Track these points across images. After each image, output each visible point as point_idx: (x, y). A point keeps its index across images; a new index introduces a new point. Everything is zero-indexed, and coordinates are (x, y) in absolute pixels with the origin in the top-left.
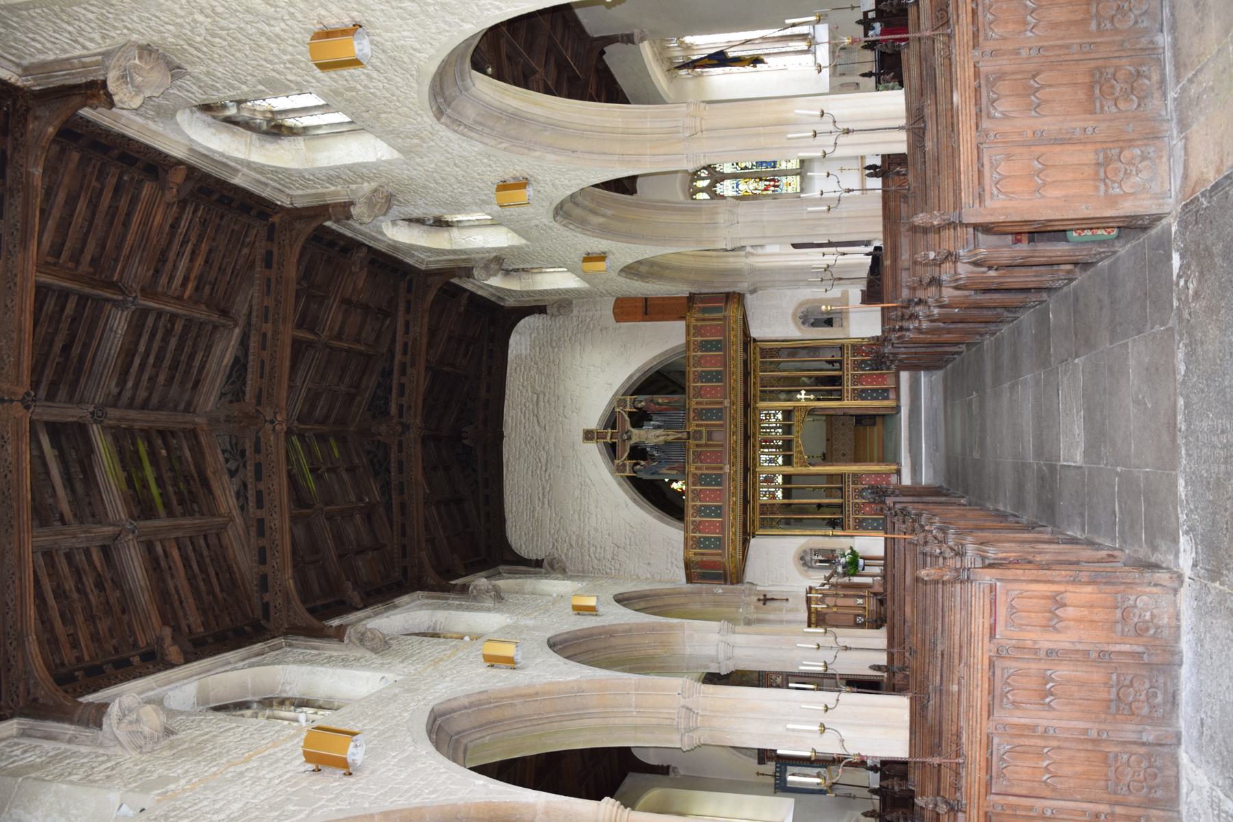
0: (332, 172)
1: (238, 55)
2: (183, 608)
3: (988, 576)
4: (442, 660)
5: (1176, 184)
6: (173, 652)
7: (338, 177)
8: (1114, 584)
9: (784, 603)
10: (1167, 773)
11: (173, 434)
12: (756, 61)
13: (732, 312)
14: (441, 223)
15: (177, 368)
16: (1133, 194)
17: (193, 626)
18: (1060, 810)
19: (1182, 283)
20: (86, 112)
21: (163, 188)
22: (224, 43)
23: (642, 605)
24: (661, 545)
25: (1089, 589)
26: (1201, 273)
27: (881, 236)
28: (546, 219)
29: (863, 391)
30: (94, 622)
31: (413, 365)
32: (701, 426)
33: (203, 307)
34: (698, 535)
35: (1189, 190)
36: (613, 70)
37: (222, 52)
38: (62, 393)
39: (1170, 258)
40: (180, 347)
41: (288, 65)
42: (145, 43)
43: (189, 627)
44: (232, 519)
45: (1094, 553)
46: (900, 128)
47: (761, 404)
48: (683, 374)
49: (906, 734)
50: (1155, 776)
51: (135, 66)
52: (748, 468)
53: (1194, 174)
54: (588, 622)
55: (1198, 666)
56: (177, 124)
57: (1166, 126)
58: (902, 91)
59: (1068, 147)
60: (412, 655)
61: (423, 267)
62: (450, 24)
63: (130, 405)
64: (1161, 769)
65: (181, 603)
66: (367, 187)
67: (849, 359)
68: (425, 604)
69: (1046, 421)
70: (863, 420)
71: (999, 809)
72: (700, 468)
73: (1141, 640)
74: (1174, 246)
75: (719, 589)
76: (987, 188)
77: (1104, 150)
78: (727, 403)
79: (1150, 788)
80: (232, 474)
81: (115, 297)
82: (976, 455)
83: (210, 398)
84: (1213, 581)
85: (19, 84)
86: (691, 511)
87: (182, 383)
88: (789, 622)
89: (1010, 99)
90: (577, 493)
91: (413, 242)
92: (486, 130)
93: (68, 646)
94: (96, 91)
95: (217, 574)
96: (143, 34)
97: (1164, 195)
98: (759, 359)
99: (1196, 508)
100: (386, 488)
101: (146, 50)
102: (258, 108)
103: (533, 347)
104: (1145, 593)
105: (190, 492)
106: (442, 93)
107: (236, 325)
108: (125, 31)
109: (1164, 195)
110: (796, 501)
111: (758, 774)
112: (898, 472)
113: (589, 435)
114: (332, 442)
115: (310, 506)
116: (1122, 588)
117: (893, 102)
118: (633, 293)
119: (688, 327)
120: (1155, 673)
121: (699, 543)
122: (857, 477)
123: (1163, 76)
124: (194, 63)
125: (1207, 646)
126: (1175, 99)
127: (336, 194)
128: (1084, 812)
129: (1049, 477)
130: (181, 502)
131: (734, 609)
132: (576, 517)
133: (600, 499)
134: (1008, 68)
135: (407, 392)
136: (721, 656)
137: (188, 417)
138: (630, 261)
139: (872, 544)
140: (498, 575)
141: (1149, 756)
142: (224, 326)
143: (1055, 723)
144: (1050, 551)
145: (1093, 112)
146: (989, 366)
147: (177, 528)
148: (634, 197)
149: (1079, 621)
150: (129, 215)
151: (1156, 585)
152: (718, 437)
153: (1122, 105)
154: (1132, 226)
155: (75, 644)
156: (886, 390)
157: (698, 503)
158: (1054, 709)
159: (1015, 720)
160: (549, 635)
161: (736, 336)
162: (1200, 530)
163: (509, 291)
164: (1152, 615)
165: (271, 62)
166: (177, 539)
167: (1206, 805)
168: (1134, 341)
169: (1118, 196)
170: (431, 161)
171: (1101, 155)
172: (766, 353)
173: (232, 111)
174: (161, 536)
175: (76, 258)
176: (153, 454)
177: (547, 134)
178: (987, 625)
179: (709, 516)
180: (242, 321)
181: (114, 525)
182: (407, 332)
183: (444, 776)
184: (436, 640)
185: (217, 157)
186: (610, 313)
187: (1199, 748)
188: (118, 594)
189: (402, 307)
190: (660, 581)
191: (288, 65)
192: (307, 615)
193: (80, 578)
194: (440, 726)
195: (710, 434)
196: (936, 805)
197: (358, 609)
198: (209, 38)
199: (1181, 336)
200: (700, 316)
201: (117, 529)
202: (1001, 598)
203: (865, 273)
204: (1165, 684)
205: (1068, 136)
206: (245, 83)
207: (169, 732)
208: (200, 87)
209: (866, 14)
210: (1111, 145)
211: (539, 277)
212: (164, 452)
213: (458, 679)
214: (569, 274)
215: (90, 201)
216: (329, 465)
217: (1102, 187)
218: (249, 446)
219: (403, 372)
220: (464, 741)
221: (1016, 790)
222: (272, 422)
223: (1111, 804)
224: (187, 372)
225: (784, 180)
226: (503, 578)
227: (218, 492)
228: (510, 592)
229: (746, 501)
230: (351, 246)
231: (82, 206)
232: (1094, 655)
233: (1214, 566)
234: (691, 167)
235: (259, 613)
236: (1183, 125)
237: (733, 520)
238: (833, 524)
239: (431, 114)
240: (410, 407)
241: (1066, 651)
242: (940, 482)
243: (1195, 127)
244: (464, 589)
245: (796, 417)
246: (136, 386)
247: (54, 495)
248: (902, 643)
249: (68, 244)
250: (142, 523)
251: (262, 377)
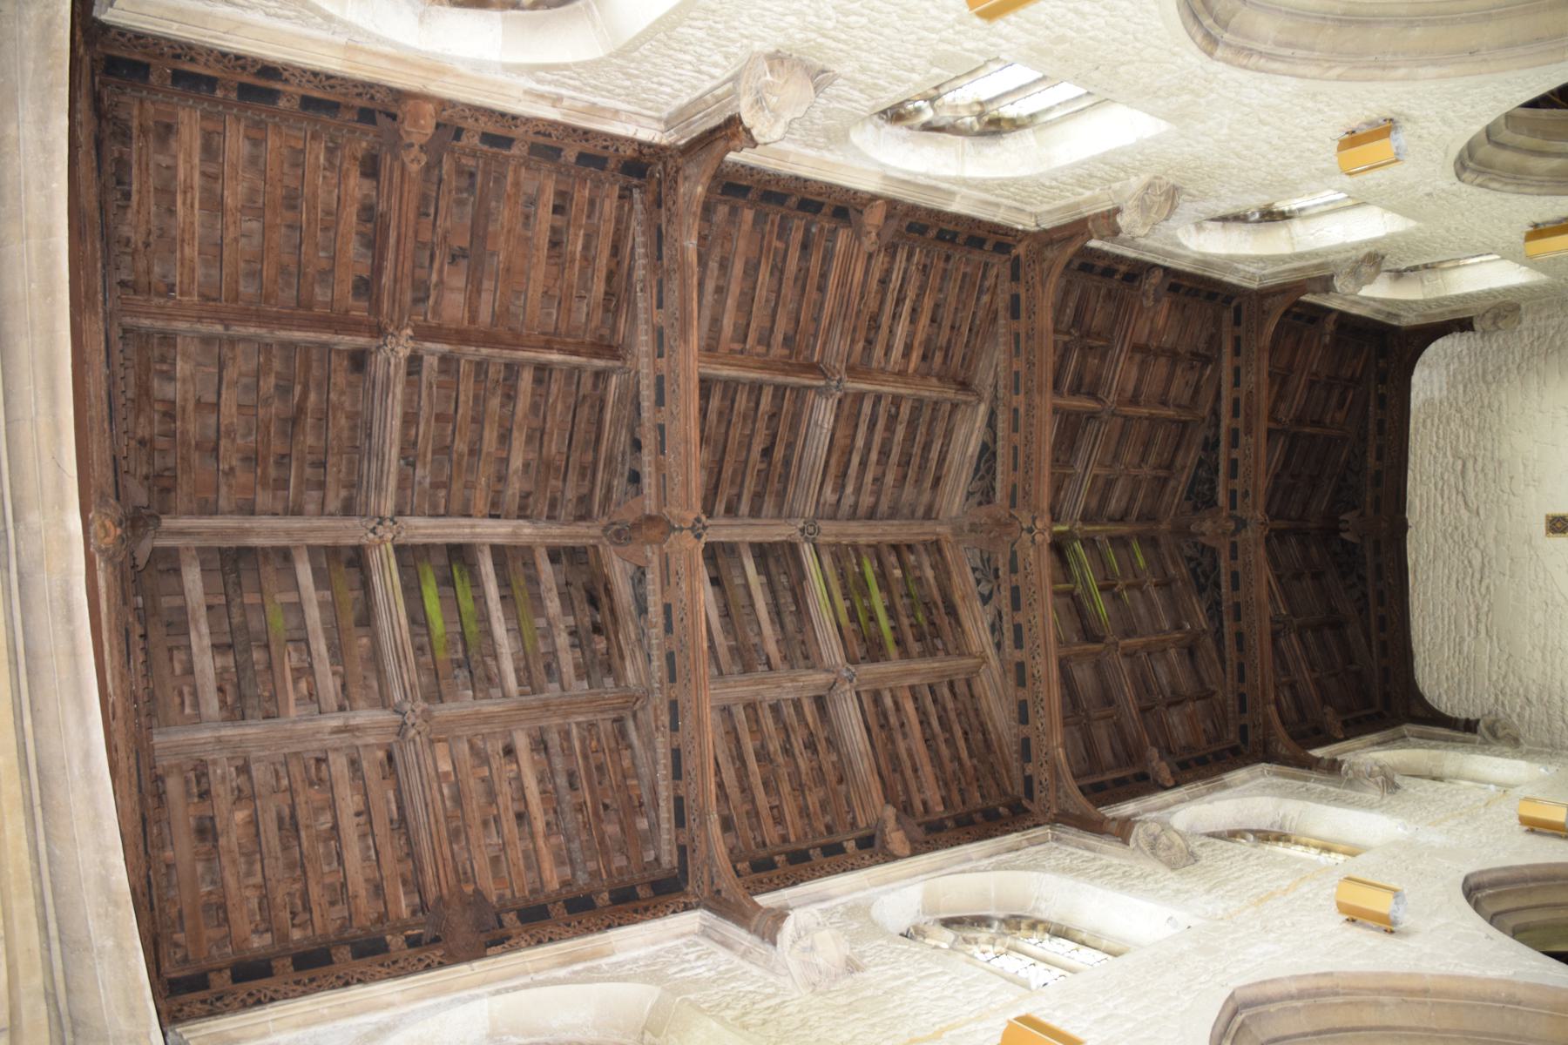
0: (1079, 171)
1: (887, 31)
2: (917, 777)
6: (896, 839)
7: (1091, 176)
11: (910, 547)
14: (1271, 216)
15: (908, 463)
17: (931, 803)
20: (732, 156)
21: (858, 236)
22: (864, 21)
28: (1445, 180)
30: (803, 792)
31: (1249, 431)
33: (934, 381)
37: (866, 34)
38: (769, 505)
40: (910, 437)
41: (958, 28)
42: (772, 49)
43: (925, 803)
44: (985, 660)
51: (767, 84)
56: (857, 148)
61: (1255, 285)
63: (853, 516)
65: (915, 770)
66: (1136, 183)
68: (1271, 786)
80: (985, 600)
81: (815, 383)
83: (954, 498)
85: (664, 142)
87: (918, 482)
90: (1538, 617)
91: (1233, 251)
92: (1300, 53)
93: (770, 821)
94: (731, 130)
95: (965, 733)
96: (763, 39)
100: (1214, 610)
101: (777, 59)
102: (959, 102)
103: (1452, 385)
105: (932, 624)
107: (980, 400)
108: (745, 41)
114: (1135, 545)
115: (1098, 639)
124: (838, 61)
127: (1094, 201)
130: (920, 638)
132: (1538, 655)
135: (1241, 470)
137: (929, 526)
140: (1400, 740)
142: (966, 403)
147: (912, 673)
150: (824, 276)
155: (779, 820)
163: (1406, 302)
165: (932, 30)
166: (912, 688)
173: (928, 115)
174: (891, 684)
175: (765, 340)
176: (882, 576)
180: (987, 395)
181: (827, 671)
182: (1237, 384)
185: (922, 180)
188: (834, 758)
189: (1227, 349)
191: (958, 28)
192: (1081, 799)
193: (788, 737)
194: (1242, 1025)
197: (1166, 788)
198: (842, 19)
201: (831, 677)
206: (913, 70)
207: (852, 966)
208: (861, 91)
211: (1455, 274)
212: (898, 573)
214: (1507, 264)
215: (774, 267)
216: (1131, 580)
218: (1002, 564)
219: (1234, 443)
222: (1030, 531)
224: (922, 467)
227: (968, 624)
230: (1137, 271)
231: (764, 275)
235: (1019, 789)
239: (1194, 48)
240: (1246, 494)
244: (1333, 767)
246: (858, 490)
247: (760, 633)
249: (753, 325)
250: (864, 667)
251: (1015, 469)
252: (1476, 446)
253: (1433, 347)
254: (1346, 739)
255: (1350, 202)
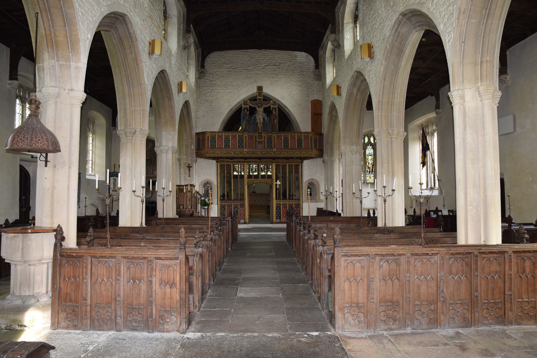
3: (182, 257)
4: (152, 20)
5: (347, 334)
8: (180, 307)
9: (188, 175)
10: (105, 326)
12: (424, 163)
13: (314, 152)
14: (356, 18)
16: (344, 317)
18: (86, 285)
19: (305, 336)
23: (185, 113)
24: (211, 120)
25: (178, 298)
26: (308, 343)
27: (345, 216)
28: (355, 68)
29: (280, 208)
32: (265, 139)
34: (217, 137)
35: (344, 339)
36: (424, 100)
39: (317, 331)
45: (197, 300)
46: (385, 223)
47: (274, 165)
48: (289, 131)
49: (128, 225)
50: (104, 322)
52: (246, 159)
53: (350, 341)
54: (174, 89)
55: (148, 339)
57: (372, 330)
58: (404, 225)
59: (366, 292)
60: (153, 6)
61: (336, 10)
62: (443, 18)
64: (106, 324)
67: (293, 203)
69: (257, 282)
70: (268, 208)
71: (85, 261)
72: (246, 139)
73: (158, 317)
74: (322, 333)
75: (193, 147)
76: (350, 258)
77: (364, 306)
78: (275, 150)
79: (98, 320)
82: (248, 254)
84: (181, 345)
86: (227, 134)
88: (180, 177)
89: (388, 268)
90: (235, 83)
91: (347, 5)
92: (395, 38)
97: (343, 329)
98: (294, 164)
99: (211, 339)
103: (300, 63)
104: (177, 319)
106: (413, 16)
109: (343, 329)
110: (232, 180)
111: (115, 165)
112: (245, 223)
113: (260, 88)
116: (179, 310)
117: (400, 221)
118: (324, 108)
119: (308, 133)
120: (145, 323)
121: (213, 138)
122: (243, 206)
123: (394, 330)
125: (154, 342)
126: (383, 334)
128: (86, 295)
129: (234, 283)
131: (184, 153)
132: (224, 83)
133: (232, 95)
134: (402, 268)
136: (162, 148)
138: (337, 107)
139: (214, 212)
140: (196, 48)
141: (112, 320)
143: (122, 284)
144: (197, 282)
145: (380, 302)
146: (285, 260)
148: (365, 109)
149: (165, 293)
151: (180, 323)
152: (260, 146)
153: (382, 314)
154: (332, 317)
156: (280, 218)
157: (230, 138)
158: (128, 283)
159: (122, 268)
160: (167, 70)
161: (304, 154)
162: (202, 341)
164: (168, 322)
167: (92, 340)
168: (285, 317)
169: (344, 311)
170: (383, 12)
171: (362, 305)
172: (297, 167)
177: (393, 67)
178: (161, 256)
179: (225, 142)
183: (91, 19)
184: (162, 17)
186: (315, 98)
187: (114, 338)
190: (196, 121)
195: (261, 142)
196: (90, 236)
199: (283, 335)
200: (313, 138)
202: (173, 262)
203: (329, 209)
204: (140, 326)
205: (370, 292)
209: (441, 211)
210: (366, 309)
211: (331, 65)
213: (143, 27)
217: (348, 305)
220: (112, 30)
221: (93, 268)
223: (91, 305)
225: (372, 176)
226: (195, 50)
228: (188, 53)
229: (232, 158)
232: (150, 299)
233: (186, 345)
234: (375, 133)
236: (371, 337)
237: (218, 153)
238: (223, 196)
241: (151, 288)
242: (239, 240)
243: (370, 341)
244: (188, 31)
245: (269, 180)
248: (167, 224)
252: (283, 69)
253: (312, 58)
254: (196, 33)
255: (356, 41)
